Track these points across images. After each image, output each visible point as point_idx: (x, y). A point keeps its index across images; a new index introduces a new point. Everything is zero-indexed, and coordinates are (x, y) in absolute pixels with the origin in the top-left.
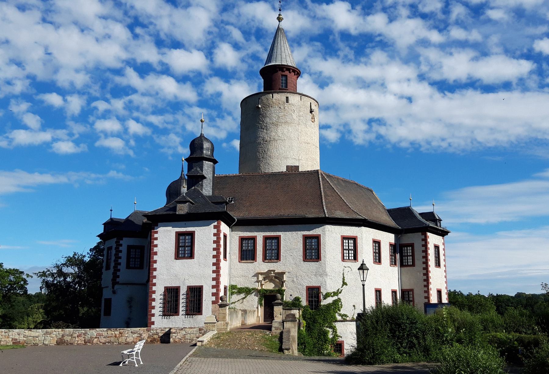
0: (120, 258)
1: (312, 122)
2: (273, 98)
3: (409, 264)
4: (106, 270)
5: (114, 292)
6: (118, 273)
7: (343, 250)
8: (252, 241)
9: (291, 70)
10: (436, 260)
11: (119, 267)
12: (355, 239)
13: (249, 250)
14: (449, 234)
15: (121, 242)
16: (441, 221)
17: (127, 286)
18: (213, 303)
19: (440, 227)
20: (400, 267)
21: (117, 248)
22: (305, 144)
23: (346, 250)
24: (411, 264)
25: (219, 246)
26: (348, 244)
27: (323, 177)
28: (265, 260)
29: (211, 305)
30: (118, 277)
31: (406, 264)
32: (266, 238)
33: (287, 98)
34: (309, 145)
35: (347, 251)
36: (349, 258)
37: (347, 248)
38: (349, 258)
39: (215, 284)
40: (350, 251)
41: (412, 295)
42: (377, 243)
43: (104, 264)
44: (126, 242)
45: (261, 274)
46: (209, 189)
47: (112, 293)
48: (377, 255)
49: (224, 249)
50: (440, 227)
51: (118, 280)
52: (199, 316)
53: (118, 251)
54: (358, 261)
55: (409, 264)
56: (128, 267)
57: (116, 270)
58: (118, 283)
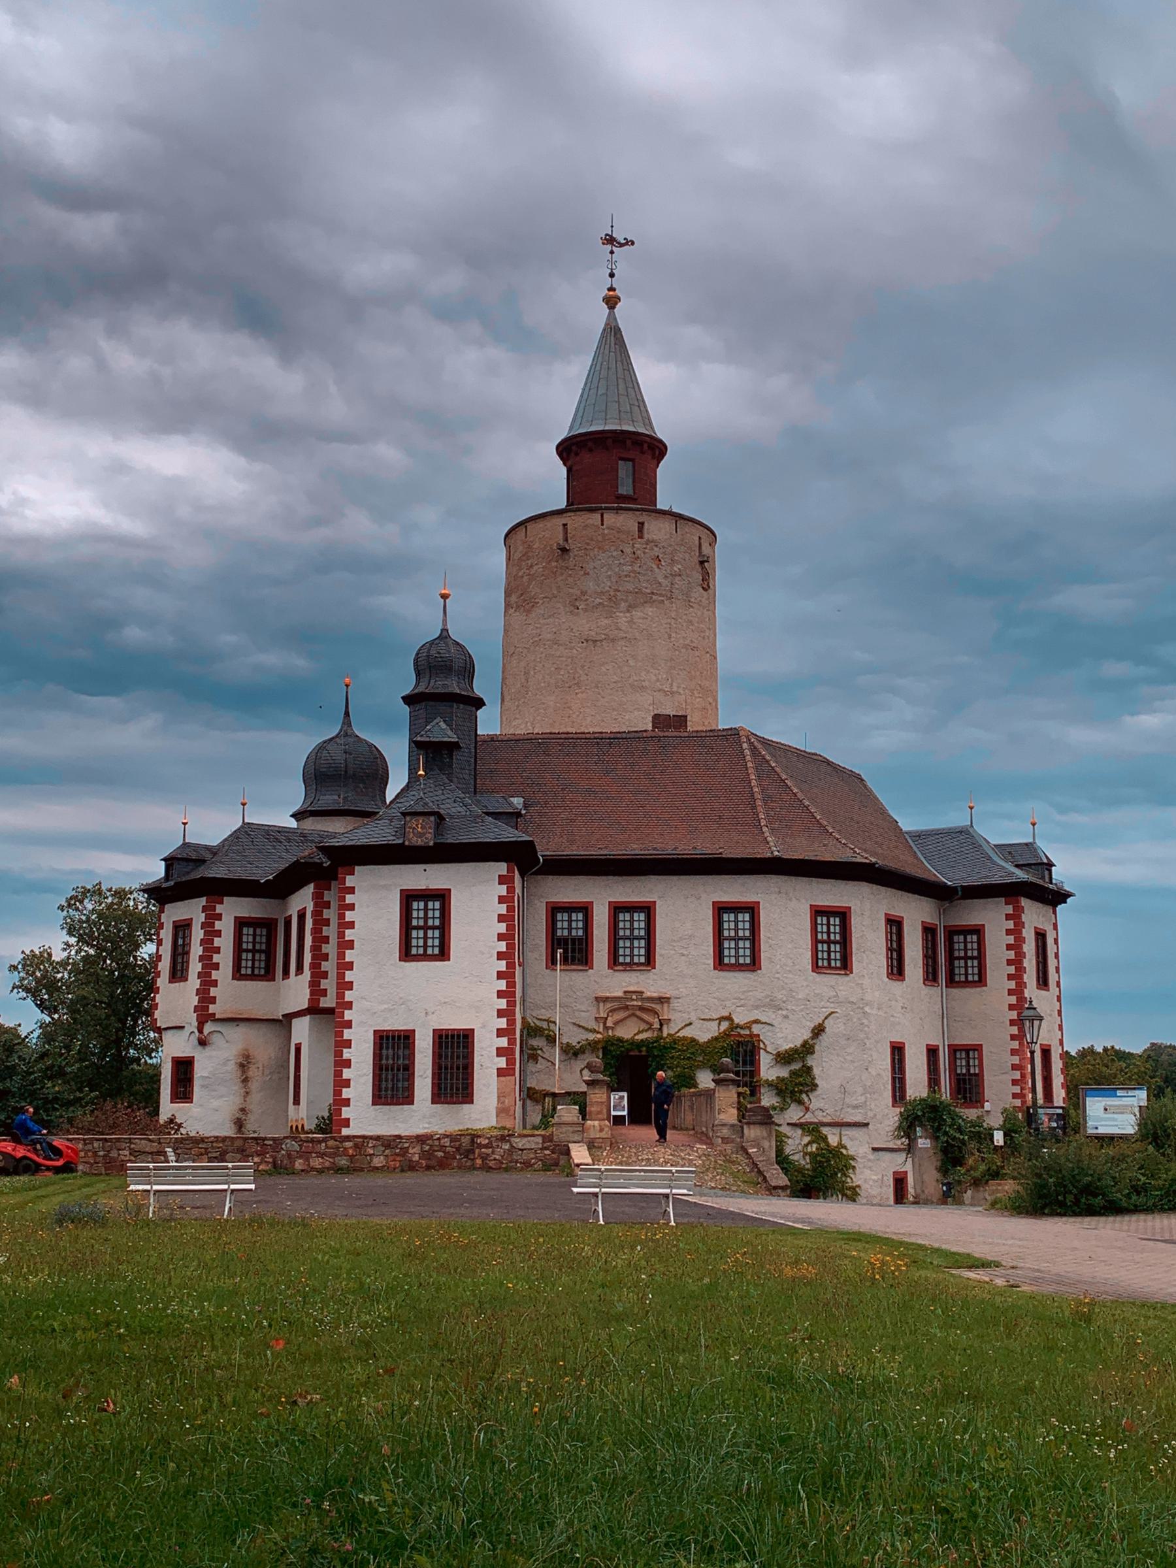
0: (218, 950)
1: (703, 588)
2: (602, 525)
3: (970, 978)
5: (203, 1043)
6: (213, 992)
7: (815, 941)
9: (645, 446)
10: (927, 965)
11: (215, 975)
13: (574, 940)
14: (1068, 900)
15: (219, 909)
16: (1053, 868)
18: (501, 1073)
19: (1051, 883)
20: (946, 986)
21: (317, 913)
22: (687, 649)
23: (823, 942)
25: (316, 948)
26: (829, 928)
27: (754, 749)
28: (615, 964)
29: (496, 1078)
30: (213, 1000)
31: (421, 951)
32: (617, 909)
33: (641, 525)
34: (697, 653)
35: (825, 946)
36: (829, 963)
38: (829, 963)
39: (505, 1026)
40: (832, 946)
41: (977, 1061)
42: (895, 925)
43: (165, 966)
44: (231, 909)
45: (605, 1000)
46: (465, 776)
47: (196, 1042)
50: (1051, 883)
51: (212, 1008)
52: (466, 1107)
53: (211, 933)
54: (852, 973)
55: (970, 978)
56: (238, 974)
57: (207, 982)
58: (212, 1017)
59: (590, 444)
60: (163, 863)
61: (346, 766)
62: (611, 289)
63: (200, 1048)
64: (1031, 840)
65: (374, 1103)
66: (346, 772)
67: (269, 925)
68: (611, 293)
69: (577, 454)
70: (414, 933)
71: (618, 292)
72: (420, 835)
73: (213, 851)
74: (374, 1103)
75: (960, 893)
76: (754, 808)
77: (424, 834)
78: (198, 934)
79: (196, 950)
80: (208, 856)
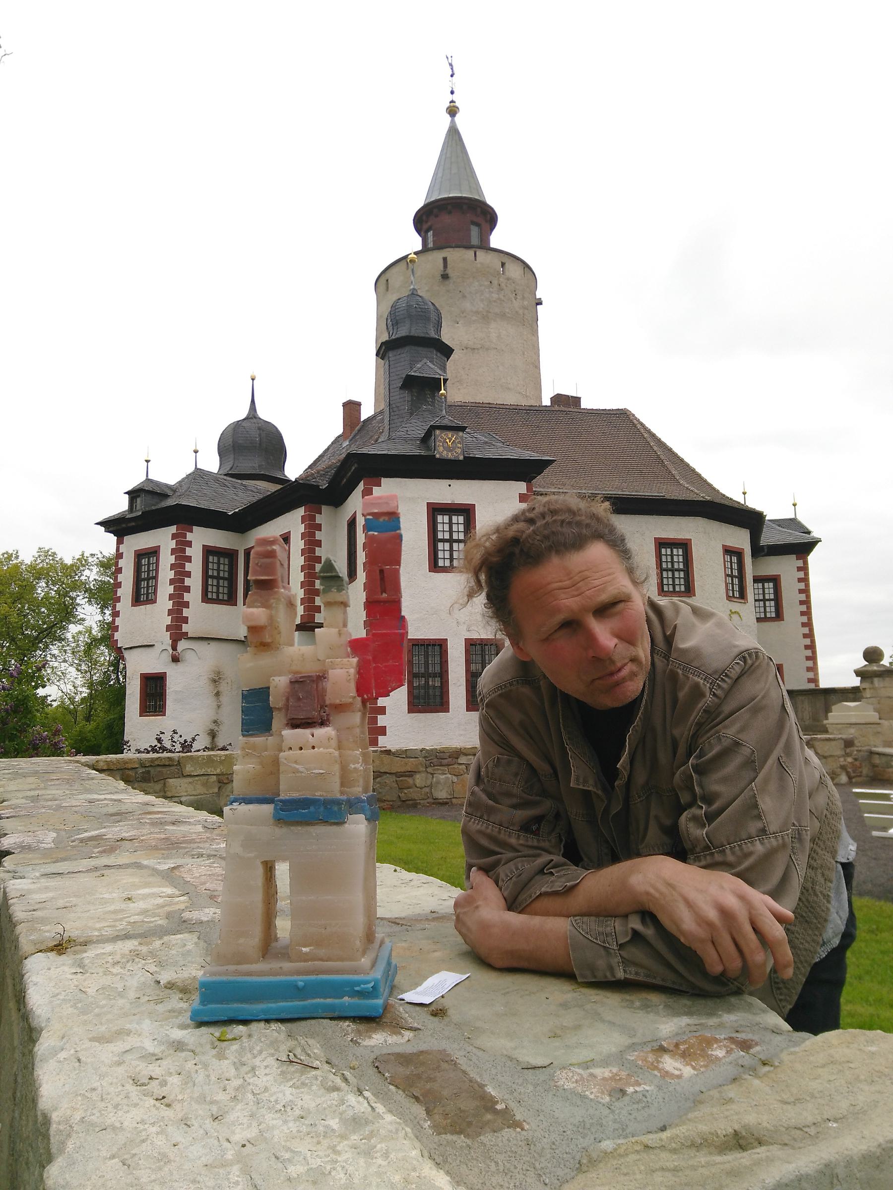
0: (188, 574)
4: (137, 600)
5: (175, 659)
6: (186, 612)
8: (771, 585)
12: (685, 546)
15: (189, 536)
17: (209, 644)
23: (667, 570)
24: (773, 615)
30: (186, 620)
33: (445, 259)
37: (670, 566)
48: (736, 581)
49: (353, 569)
51: (185, 628)
55: (768, 615)
56: (206, 599)
58: (185, 636)
59: (449, 207)
60: (127, 496)
61: (260, 440)
62: (452, 102)
63: (174, 664)
64: (793, 516)
65: (410, 711)
66: (260, 444)
67: (230, 555)
68: (452, 104)
69: (437, 216)
70: (440, 546)
71: (457, 104)
72: (449, 449)
73: (173, 489)
74: (410, 711)
75: (766, 550)
76: (664, 466)
77: (454, 448)
78: (167, 559)
79: (166, 574)
80: (170, 493)
